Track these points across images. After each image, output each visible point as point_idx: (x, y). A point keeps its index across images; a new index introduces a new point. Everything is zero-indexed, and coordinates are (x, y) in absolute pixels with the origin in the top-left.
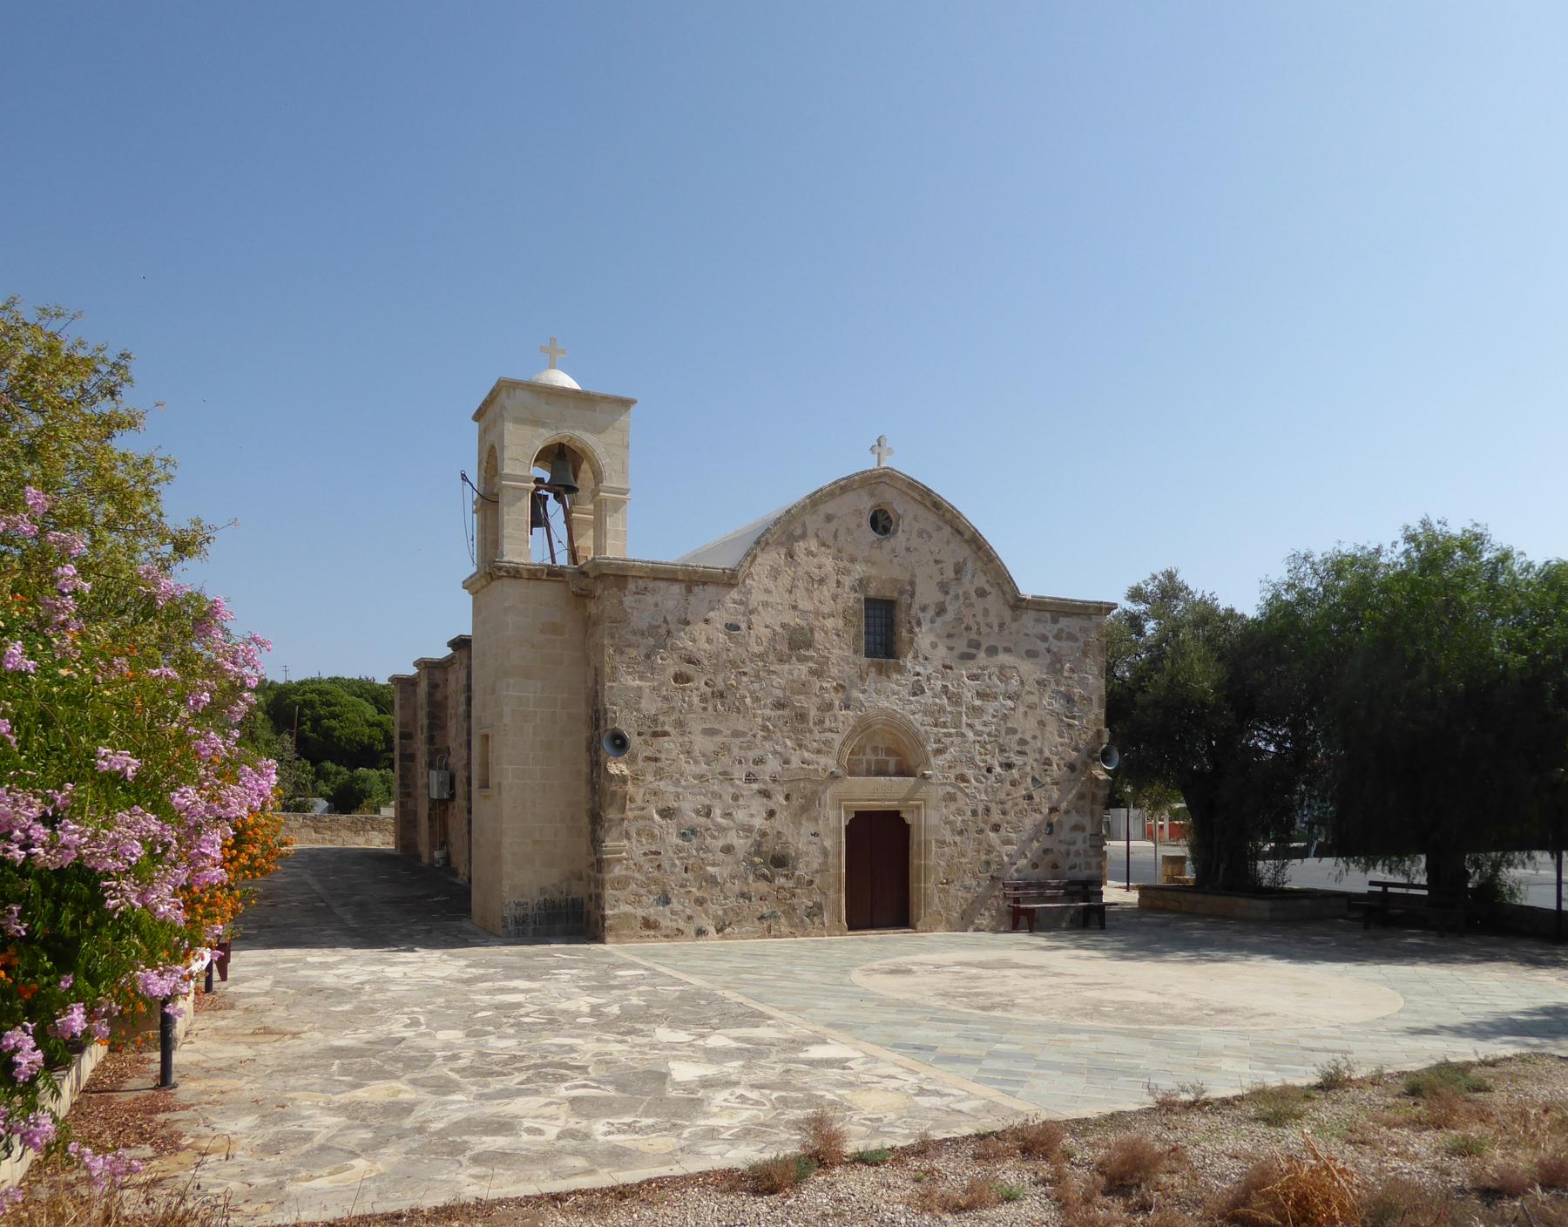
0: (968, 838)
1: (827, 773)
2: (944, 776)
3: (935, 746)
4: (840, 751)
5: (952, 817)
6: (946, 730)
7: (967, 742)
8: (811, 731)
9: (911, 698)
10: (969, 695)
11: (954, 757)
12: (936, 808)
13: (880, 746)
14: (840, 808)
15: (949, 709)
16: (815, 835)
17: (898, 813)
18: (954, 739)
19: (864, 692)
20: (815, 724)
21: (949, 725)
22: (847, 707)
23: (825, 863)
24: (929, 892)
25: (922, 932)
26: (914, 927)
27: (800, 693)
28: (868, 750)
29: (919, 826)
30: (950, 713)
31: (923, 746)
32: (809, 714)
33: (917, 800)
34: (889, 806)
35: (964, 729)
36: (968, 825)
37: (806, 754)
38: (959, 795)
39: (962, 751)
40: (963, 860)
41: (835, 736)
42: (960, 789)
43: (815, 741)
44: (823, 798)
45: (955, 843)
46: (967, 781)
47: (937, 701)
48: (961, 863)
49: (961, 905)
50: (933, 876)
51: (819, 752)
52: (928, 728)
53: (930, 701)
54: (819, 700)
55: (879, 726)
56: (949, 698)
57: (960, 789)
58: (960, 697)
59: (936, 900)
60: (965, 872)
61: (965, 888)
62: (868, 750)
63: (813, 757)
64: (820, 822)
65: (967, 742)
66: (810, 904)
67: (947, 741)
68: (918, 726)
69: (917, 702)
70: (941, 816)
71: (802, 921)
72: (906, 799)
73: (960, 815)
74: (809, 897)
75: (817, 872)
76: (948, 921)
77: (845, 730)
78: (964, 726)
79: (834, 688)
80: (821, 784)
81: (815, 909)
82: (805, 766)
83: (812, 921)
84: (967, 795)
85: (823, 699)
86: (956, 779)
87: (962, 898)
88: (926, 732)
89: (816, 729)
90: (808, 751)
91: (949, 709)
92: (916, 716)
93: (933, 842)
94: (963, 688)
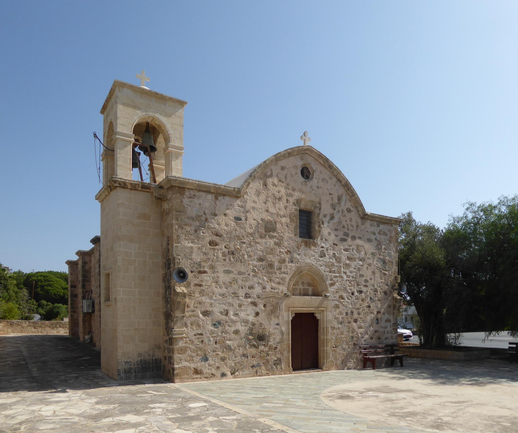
0: (344, 326)
3: (330, 282)
5: (337, 316)
6: (335, 274)
8: (275, 273)
9: (320, 259)
10: (344, 258)
12: (331, 311)
13: (305, 281)
16: (278, 324)
18: (338, 279)
19: (299, 254)
20: (277, 269)
21: (336, 272)
22: (292, 262)
24: (328, 351)
25: (325, 371)
26: (321, 369)
28: (300, 284)
29: (323, 320)
30: (337, 266)
31: (325, 282)
32: (274, 264)
37: (273, 285)
38: (341, 305)
39: (341, 285)
40: (342, 336)
42: (341, 302)
43: (277, 278)
45: (339, 328)
46: (344, 299)
47: (331, 260)
48: (341, 337)
49: (342, 357)
50: (330, 344)
51: (279, 283)
52: (327, 273)
53: (328, 260)
54: (279, 258)
55: (306, 272)
56: (336, 259)
57: (341, 302)
60: (343, 341)
61: (343, 349)
66: (276, 359)
67: (335, 279)
69: (323, 260)
74: (275, 356)
75: (279, 343)
76: (336, 365)
77: (291, 273)
80: (280, 299)
82: (273, 290)
83: (277, 367)
84: (344, 305)
85: (281, 257)
88: (326, 275)
89: (278, 272)
90: (274, 283)
92: (322, 267)
93: (330, 327)
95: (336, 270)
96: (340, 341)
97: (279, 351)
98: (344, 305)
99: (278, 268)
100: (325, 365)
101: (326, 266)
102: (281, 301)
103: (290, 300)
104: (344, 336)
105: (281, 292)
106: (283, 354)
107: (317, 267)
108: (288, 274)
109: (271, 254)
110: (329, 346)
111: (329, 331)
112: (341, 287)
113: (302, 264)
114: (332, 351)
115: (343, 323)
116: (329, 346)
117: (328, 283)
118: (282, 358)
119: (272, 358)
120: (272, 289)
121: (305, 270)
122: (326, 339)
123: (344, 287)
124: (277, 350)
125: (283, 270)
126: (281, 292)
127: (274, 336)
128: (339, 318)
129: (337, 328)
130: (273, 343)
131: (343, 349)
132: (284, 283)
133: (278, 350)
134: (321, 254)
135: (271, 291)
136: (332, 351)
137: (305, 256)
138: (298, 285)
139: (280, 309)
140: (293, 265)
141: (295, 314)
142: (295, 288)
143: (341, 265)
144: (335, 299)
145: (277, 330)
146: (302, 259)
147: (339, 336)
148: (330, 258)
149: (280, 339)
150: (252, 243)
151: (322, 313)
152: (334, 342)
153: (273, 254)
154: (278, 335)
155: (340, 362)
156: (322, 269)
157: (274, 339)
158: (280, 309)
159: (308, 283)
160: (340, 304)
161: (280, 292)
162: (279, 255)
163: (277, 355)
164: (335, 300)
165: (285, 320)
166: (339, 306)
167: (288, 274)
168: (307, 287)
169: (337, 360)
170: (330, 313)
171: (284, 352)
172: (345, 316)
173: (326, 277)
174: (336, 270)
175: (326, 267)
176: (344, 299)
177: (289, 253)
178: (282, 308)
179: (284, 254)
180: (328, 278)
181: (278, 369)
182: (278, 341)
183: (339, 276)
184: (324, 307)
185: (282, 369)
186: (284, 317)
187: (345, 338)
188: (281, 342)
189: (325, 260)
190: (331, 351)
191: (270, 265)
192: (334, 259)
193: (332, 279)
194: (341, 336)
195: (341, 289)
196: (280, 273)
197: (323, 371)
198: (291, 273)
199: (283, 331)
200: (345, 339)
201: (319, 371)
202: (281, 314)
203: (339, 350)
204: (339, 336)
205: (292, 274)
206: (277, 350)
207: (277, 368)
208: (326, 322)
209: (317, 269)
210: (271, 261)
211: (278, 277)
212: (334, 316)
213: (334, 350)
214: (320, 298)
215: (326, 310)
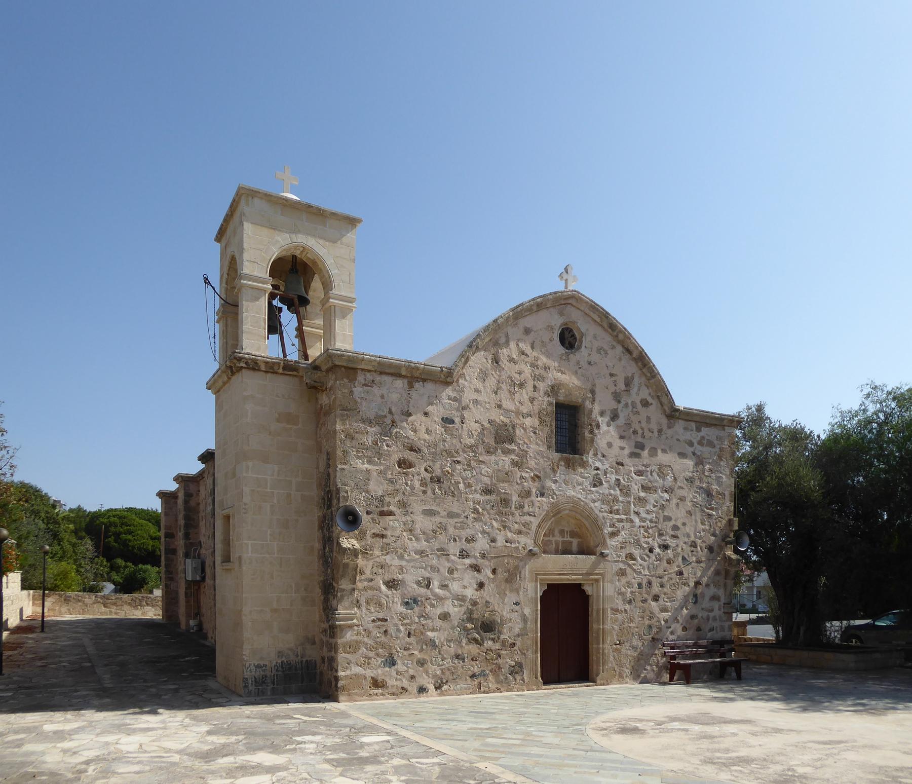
0: (635, 607)
3: (610, 530)
5: (623, 589)
6: (618, 517)
8: (513, 515)
9: (593, 489)
10: (636, 487)
12: (612, 582)
13: (566, 529)
14: (537, 581)
16: (517, 604)
19: (555, 482)
20: (516, 508)
21: (620, 512)
22: (542, 495)
24: (606, 651)
25: (601, 685)
26: (594, 681)
29: (598, 596)
30: (622, 502)
37: (509, 535)
38: (629, 570)
39: (631, 535)
40: (632, 625)
41: (532, 519)
42: (629, 565)
43: (516, 523)
45: (626, 610)
46: (634, 559)
47: (612, 492)
48: (630, 627)
52: (605, 514)
53: (607, 492)
55: (567, 512)
56: (621, 490)
57: (629, 565)
60: (633, 634)
61: (633, 648)
62: (556, 532)
66: (513, 663)
68: (597, 512)
69: (597, 492)
71: (506, 678)
74: (512, 657)
75: (518, 635)
78: (632, 513)
80: (521, 561)
82: (508, 544)
83: (514, 678)
84: (634, 570)
85: (523, 487)
88: (604, 518)
89: (517, 513)
90: (511, 531)
92: (596, 504)
93: (609, 609)
96: (628, 633)
97: (519, 650)
100: (600, 676)
101: (603, 502)
102: (523, 562)
106: (525, 655)
107: (586, 503)
108: (535, 516)
111: (608, 616)
114: (613, 652)
115: (633, 601)
118: (524, 663)
119: (507, 662)
121: (565, 510)
122: (603, 629)
123: (636, 538)
124: (515, 648)
125: (526, 509)
126: (523, 547)
129: (621, 611)
134: (593, 480)
138: (553, 536)
140: (544, 499)
141: (548, 585)
142: (549, 541)
143: (629, 499)
144: (618, 559)
145: (516, 613)
146: (560, 491)
147: (626, 625)
148: (610, 488)
149: (521, 629)
152: (617, 635)
153: (509, 482)
157: (510, 629)
158: (520, 577)
159: (570, 532)
162: (519, 482)
163: (516, 657)
164: (619, 561)
165: (529, 596)
167: (535, 516)
170: (609, 585)
171: (527, 650)
172: (637, 590)
174: (621, 508)
175: (604, 504)
176: (634, 559)
180: (606, 523)
181: (518, 681)
183: (627, 518)
184: (599, 574)
185: (524, 682)
187: (637, 628)
189: (601, 492)
190: (611, 651)
192: (617, 489)
194: (630, 625)
198: (541, 514)
201: (589, 686)
203: (626, 649)
204: (626, 625)
205: (542, 517)
207: (516, 680)
210: (505, 493)
211: (518, 521)
213: (616, 649)
215: (603, 579)
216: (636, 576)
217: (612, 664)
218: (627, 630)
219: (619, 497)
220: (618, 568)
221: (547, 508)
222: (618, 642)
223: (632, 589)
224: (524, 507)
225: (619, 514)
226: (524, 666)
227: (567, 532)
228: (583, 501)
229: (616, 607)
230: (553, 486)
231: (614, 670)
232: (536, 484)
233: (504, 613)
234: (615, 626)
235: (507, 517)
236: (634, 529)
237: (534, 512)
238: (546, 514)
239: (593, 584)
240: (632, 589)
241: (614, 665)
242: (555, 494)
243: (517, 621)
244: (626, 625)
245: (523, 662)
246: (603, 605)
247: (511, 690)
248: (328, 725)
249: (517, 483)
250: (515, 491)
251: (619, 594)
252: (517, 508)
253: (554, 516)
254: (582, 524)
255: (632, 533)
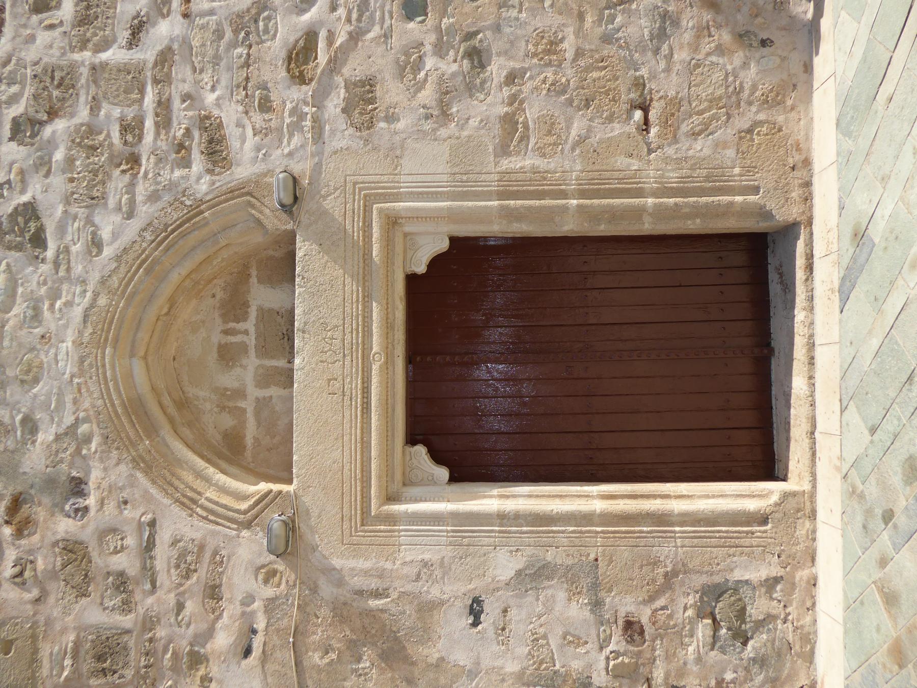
0: (497, 28)
1: (280, 566)
2: (296, 127)
3: (198, 164)
4: (213, 515)
5: (427, 95)
6: (149, 124)
7: (185, 42)
8: (149, 623)
9: (50, 253)
10: (43, 37)
11: (233, 89)
12: (395, 154)
13: (217, 338)
14: (391, 519)
15: (83, 114)
16: (475, 611)
17: (412, 280)
18: (176, 90)
19: (30, 426)
20: (126, 607)
21: (130, 113)
22: (78, 487)
23: (570, 576)
24: (673, 176)
25: (808, 199)
26: (790, 231)
27: (34, 660)
28: (228, 380)
29: (452, 216)
30: (95, 108)
31: (197, 209)
32: (98, 628)
33: (368, 236)
34: (388, 326)
35: (147, 54)
36: (451, 31)
37: (223, 640)
38: (354, 68)
39: (216, 60)
40: (569, 46)
41: (164, 536)
42: (335, 64)
43: (180, 607)
44: (357, 582)
45: (512, 78)
46: (311, 37)
47: (59, 156)
48: (579, 53)
49: (720, 50)
50: (621, 161)
51: (213, 592)
52: (142, 190)
53: (58, 181)
54: (56, 588)
55: (138, 368)
56: (53, 114)
57: (335, 64)
58: (51, 71)
59: (701, 147)
60: (607, 39)
61: (661, 35)
62: (228, 380)
63: (231, 611)
64: (435, 592)
65: (185, 42)
66: (703, 629)
67: (182, 116)
68: (135, 225)
69: (61, 229)
70: (422, 135)
71: (761, 661)
72: (365, 274)
73: (418, 66)
74: (681, 635)
75: (597, 604)
76: (772, 100)
77: (147, 498)
78: (136, 55)
79: (19, 533)
80: (314, 590)
81: (720, 608)
82: (257, 643)
83: (759, 625)
84: (355, 37)
85: (53, 575)
86: (302, 79)
87: (695, 47)
88: (153, 197)
89: (147, 603)
90: (210, 633)
91: (83, 114)
92: (105, 234)
93: (506, 164)
94: (22, 65)
95: (117, 112)
96: (601, 63)
97: (651, 599)
98: (355, 37)
99: (117, 601)
100: (771, 205)
101: (96, 201)
102: (322, 582)
103: (314, 512)
104: (570, 31)
105: (266, 581)
106: (675, 573)
107: (103, 282)
108: (152, 524)
109: (36, 651)
110: (635, 165)
111: (535, 170)
112: (229, 69)
113: (87, 405)
114: (675, 140)
115: (476, 42)
116: (635, 165)
117: (203, 187)
118: (704, 579)
119: (699, 660)
120: (247, 652)
121: (129, 376)
122: (583, 194)
123: (229, 35)
124: (645, 620)
125: (125, 562)
126: (266, 581)
127: (554, 643)
128: (441, 79)
129: (513, 99)
130: (594, 654)
131: (661, 35)
132: (207, 555)
133: (648, 612)
134: (19, 247)
135: (265, 657)
136: (675, 140)
137: (36, 380)
138: (240, 393)
139: (377, 594)
140: (95, 475)
141: (412, 440)
142: (257, 413)
143: (85, 71)
144: (308, 123)
145: (513, 613)
146: (60, 404)
147: (569, 74)
148: (44, 165)
149: (573, 594)
150: (464, 11)
151: (408, 229)
152: (610, 119)
153: (34, 638)
154: (549, 610)
155: (753, 69)
156: (115, 236)
157: (572, 640)
158: (377, 594)
159: (225, 317)
160: (347, 71)
161: (269, 592)
162: (35, 593)
163: (679, 616)
164: (316, 120)
165: (448, 552)
166: (363, 83)
167: (152, 524)
168: (250, 325)
169: (738, 92)
170: (408, 164)
171: (655, 563)
172: (431, 20)
173: (167, 198)
174: (117, 112)
175: (104, 197)
176: (311, 37)
177: (25, 510)
178: (366, 573)
179: (30, 552)
180: (171, 186)
181: (775, 608)
182: (587, 613)
183: (156, 82)
184: (367, 210)
185: (777, 580)
186: (425, 564)
187: (581, 16)
188: (595, 587)
189: (60, 209)
190: (670, 151)
191: (100, 658)
192: (48, 131)
193: (181, 147)
194: (569, 55)
195: (247, 65)
196: (148, 586)
197: (810, 222)
198: (147, 498)
199: (519, 573)
200: (589, 19)
201: (810, 257)
202: (409, 587)
203: (668, 70)
204: (569, 74)
205: (154, 491)
206: (644, 616)
207: (770, 618)
208: (464, 196)
209: (115, 281)
210: (75, 655)
211: (171, 599)
212: (428, 126)
213: (665, 123)
214: (302, 248)
215: (386, 198)
216: (376, 31)
217: (725, 145)
218: (588, 69)
219: (77, 120)
220: (342, 123)
221: (123, 468)
222: (638, 115)
223: (428, 48)
224: (121, 574)
225: (140, 121)
226: (717, 579)
227: (226, 332)
228: (96, 295)
229: (497, 129)
230: (45, 436)
231: (750, 131)
232: (40, 513)
233: (512, 667)
234: (574, 133)
235: (160, 646)
236: (195, 43)
237: (140, 525)
238: (146, 473)
239: (406, 235)
240: (428, 48)
241: (726, 133)
242: (71, 431)
243: (540, 608)
244: (570, 72)
245: (700, 580)
246: (487, 196)
247: (809, 639)
248: (739, 93)
249: (38, 600)
250: (66, 612)
251: (445, 115)
252: (125, 602)
253: (151, 430)
254: (188, 283)
255: (210, 52)
